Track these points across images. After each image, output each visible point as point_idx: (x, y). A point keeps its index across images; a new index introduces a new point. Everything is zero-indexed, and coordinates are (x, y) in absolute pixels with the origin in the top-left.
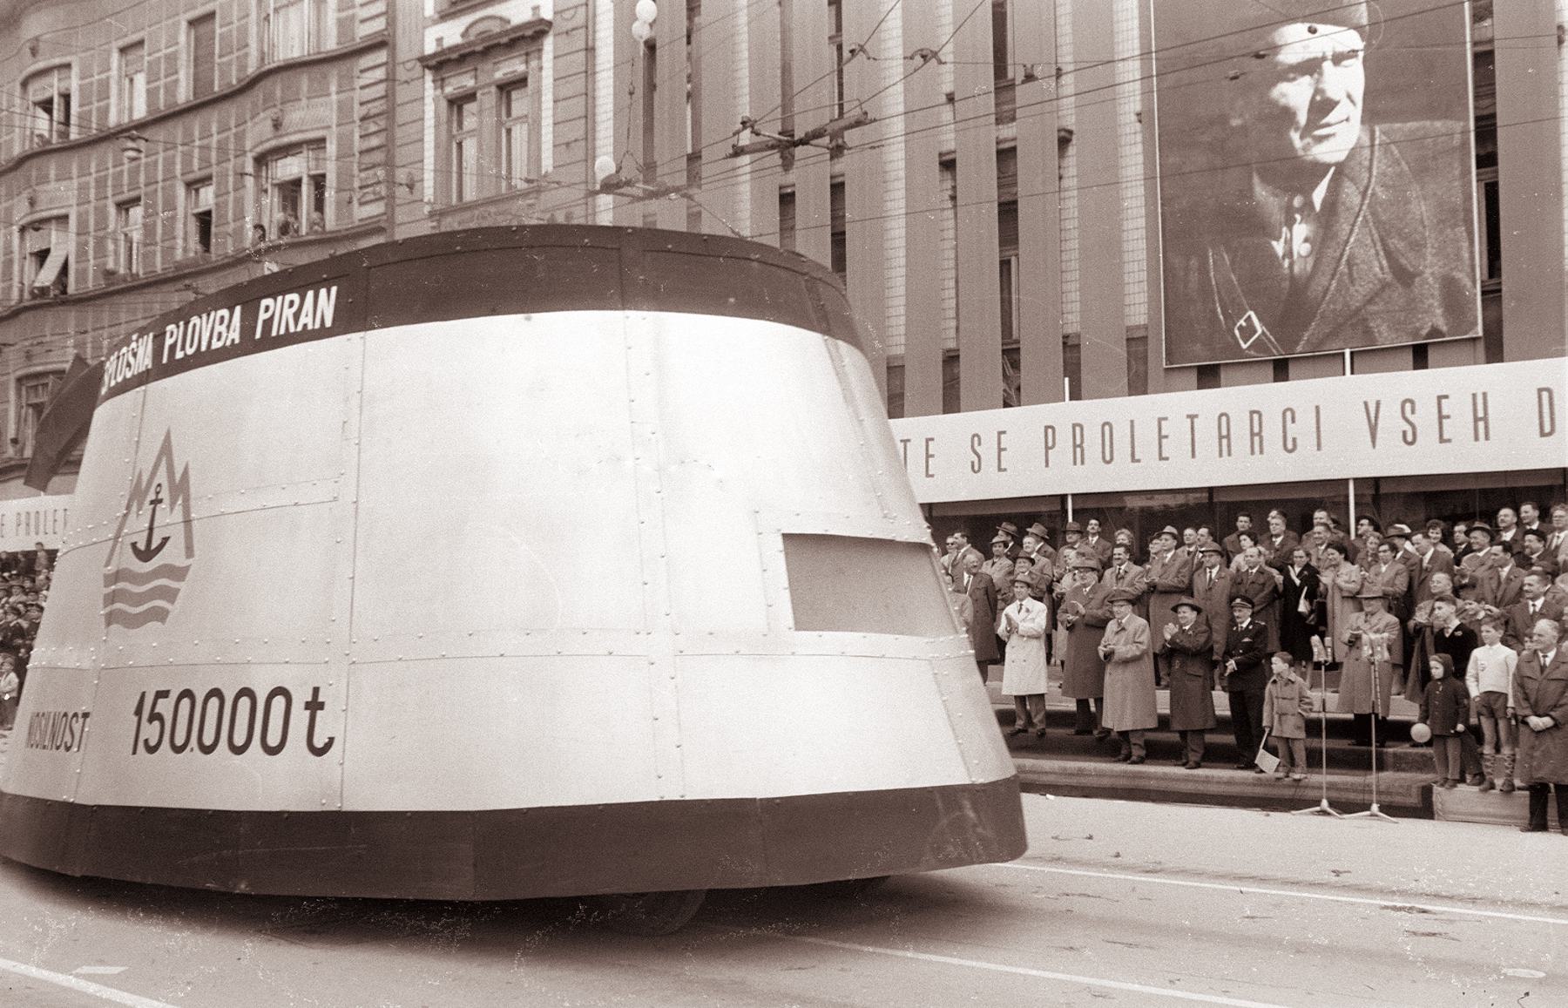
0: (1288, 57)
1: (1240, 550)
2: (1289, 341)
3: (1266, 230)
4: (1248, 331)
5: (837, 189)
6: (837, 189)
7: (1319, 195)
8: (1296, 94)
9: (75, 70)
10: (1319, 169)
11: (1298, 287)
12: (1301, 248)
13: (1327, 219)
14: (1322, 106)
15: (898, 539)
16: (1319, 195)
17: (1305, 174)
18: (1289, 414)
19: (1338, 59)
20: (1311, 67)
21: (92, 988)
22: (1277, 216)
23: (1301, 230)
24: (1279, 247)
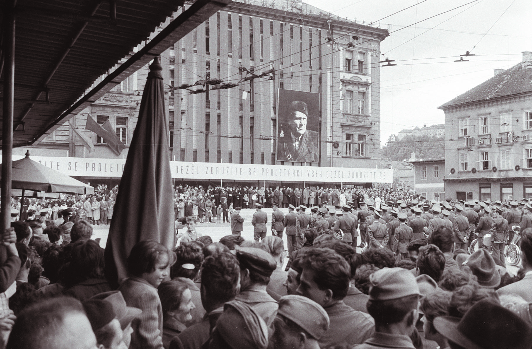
0: (297, 116)
1: (395, 260)
2: (295, 160)
3: (293, 142)
4: (289, 157)
5: (219, 116)
6: (219, 116)
7: (300, 137)
8: (298, 122)
9: (453, 260)
10: (301, 134)
11: (296, 151)
12: (297, 146)
13: (301, 142)
14: (301, 125)
15: (360, 22)
16: (300, 137)
17: (298, 135)
18: (357, 177)
19: (304, 119)
20: (300, 119)
21: (160, 213)
22: (294, 140)
23: (297, 143)
24: (294, 145)
